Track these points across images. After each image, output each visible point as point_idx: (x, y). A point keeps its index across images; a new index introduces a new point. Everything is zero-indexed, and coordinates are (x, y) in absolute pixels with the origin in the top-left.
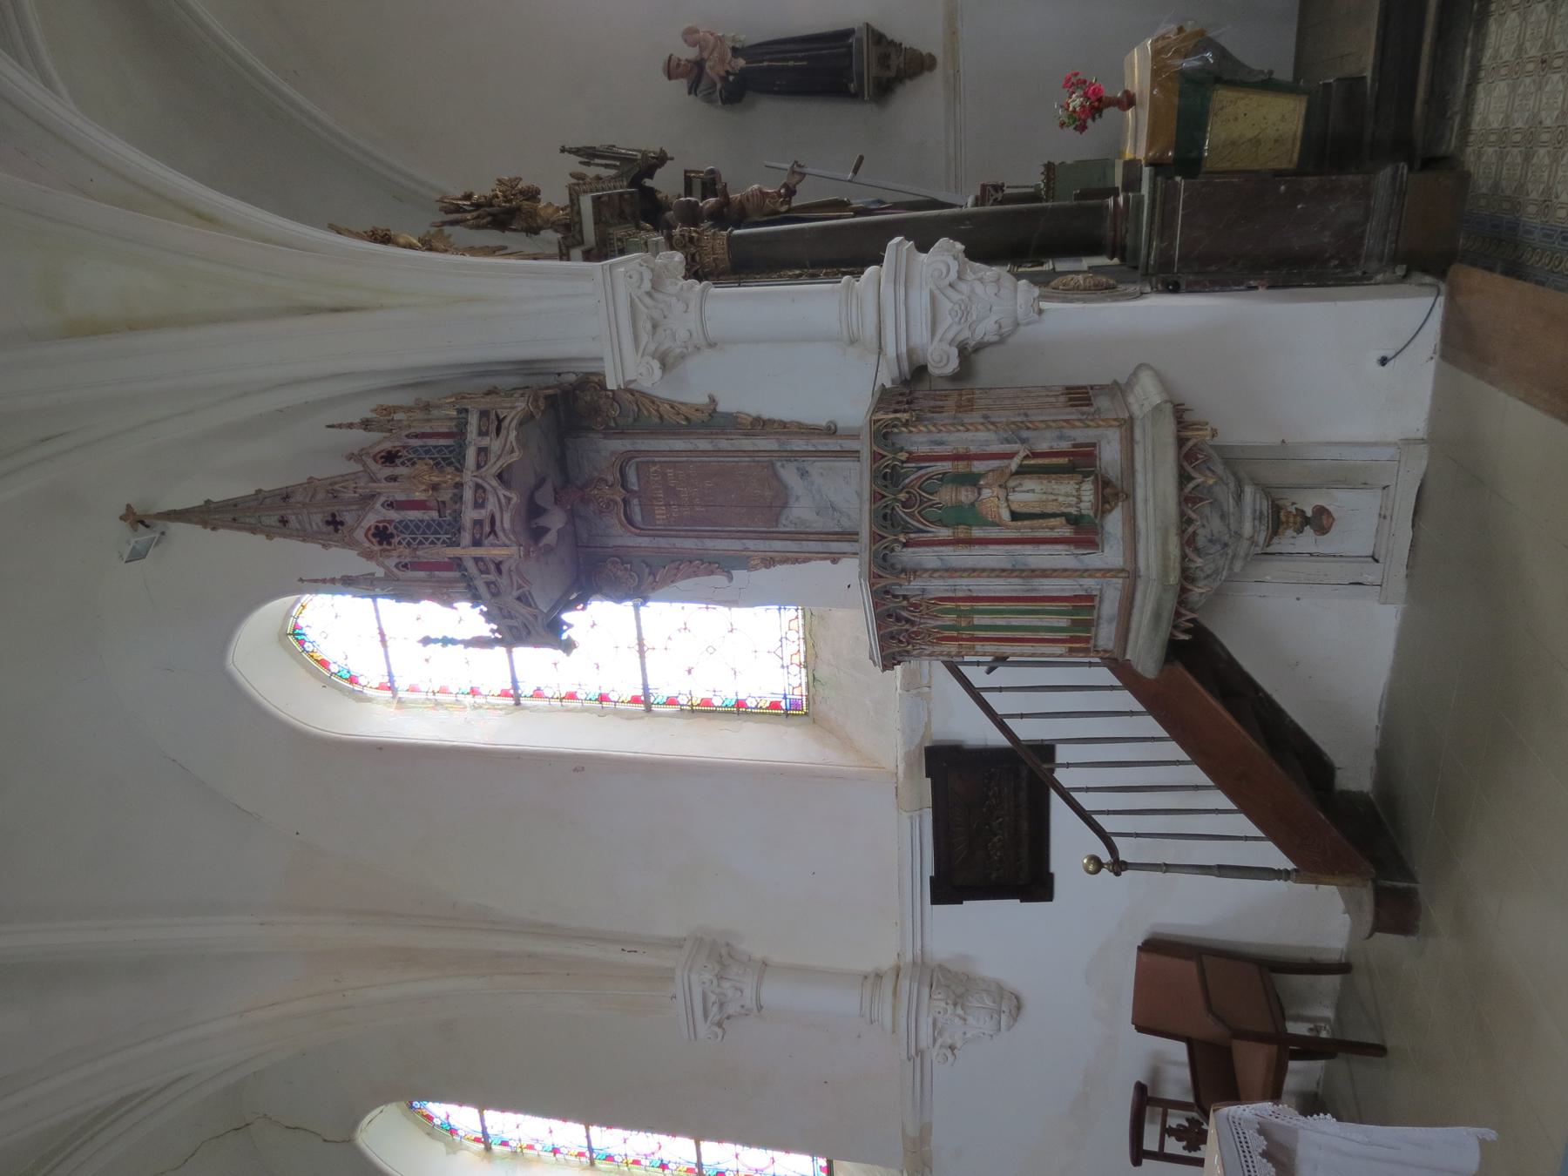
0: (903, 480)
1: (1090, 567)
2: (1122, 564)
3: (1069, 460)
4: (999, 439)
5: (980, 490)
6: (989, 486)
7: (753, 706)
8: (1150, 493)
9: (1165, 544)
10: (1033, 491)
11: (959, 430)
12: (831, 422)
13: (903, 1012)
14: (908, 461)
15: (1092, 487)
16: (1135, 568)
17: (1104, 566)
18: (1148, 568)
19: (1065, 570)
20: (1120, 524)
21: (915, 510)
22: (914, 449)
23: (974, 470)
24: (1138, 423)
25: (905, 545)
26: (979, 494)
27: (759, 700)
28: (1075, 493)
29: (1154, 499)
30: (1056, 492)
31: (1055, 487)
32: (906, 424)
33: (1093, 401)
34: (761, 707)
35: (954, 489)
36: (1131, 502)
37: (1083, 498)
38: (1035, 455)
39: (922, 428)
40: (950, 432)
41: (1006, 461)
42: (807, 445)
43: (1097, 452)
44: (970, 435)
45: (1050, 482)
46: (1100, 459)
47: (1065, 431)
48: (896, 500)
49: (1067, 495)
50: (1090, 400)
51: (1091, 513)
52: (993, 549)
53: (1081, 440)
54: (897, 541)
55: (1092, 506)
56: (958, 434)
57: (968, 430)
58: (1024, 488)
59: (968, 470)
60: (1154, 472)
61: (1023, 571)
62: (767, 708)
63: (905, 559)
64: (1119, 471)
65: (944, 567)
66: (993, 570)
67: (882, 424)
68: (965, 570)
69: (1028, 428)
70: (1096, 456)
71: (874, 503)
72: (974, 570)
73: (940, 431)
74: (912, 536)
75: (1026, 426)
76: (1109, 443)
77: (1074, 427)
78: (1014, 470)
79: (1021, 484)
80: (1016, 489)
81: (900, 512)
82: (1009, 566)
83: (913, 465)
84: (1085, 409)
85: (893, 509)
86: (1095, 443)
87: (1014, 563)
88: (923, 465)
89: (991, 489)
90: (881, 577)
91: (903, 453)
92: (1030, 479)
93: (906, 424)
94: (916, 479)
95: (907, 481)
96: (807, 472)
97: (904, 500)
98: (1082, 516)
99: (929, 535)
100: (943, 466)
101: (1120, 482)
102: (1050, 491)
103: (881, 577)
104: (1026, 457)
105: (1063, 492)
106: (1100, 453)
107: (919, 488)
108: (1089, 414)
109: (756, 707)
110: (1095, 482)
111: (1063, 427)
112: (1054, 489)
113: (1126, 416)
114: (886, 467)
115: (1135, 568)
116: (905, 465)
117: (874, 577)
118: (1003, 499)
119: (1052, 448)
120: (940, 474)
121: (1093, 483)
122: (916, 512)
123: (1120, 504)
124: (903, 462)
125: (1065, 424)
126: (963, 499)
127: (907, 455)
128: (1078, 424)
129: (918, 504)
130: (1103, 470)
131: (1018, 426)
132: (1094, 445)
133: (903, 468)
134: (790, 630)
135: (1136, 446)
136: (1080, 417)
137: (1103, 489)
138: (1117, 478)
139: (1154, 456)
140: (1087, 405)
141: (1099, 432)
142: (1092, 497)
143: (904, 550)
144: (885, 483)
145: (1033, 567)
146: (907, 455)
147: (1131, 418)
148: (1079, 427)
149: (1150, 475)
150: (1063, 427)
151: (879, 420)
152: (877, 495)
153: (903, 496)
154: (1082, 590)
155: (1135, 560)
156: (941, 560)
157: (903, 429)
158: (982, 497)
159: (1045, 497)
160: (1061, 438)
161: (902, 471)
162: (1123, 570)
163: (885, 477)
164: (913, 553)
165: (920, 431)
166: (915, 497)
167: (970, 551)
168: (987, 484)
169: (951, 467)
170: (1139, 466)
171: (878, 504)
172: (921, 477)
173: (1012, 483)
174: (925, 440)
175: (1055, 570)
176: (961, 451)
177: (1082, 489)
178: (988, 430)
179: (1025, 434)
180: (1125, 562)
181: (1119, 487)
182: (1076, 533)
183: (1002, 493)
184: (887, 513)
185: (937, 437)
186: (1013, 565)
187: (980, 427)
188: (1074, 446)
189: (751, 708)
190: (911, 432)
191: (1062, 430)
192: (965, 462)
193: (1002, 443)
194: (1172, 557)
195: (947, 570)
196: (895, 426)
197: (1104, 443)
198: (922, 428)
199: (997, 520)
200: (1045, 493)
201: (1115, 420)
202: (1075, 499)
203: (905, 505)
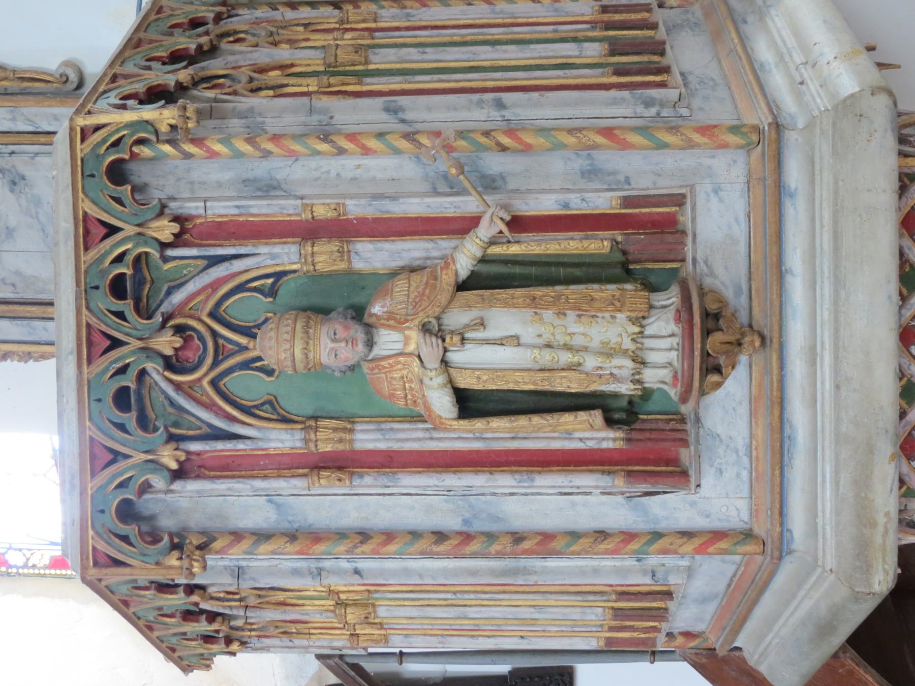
0: (169, 293)
1: (662, 526)
2: (745, 516)
3: (614, 241)
4: (426, 178)
5: (369, 329)
6: (396, 322)
7: (21, 564)
8: (825, 337)
9: (862, 482)
10: (515, 340)
11: (319, 153)
12: (67, 64)
13: (405, 622)
14: (179, 240)
15: (673, 327)
16: (781, 534)
17: (699, 522)
18: (813, 531)
19: (602, 535)
20: (744, 409)
21: (202, 376)
22: (192, 208)
23: (359, 265)
24: (792, 138)
25: (179, 474)
26: (370, 344)
27: (28, 554)
28: (628, 344)
29: (836, 358)
30: (578, 341)
31: (571, 330)
32: (174, 135)
33: (669, 59)
34: (34, 566)
35: (299, 326)
36: (775, 357)
37: (652, 357)
38: (518, 224)
39: (218, 147)
40: (293, 155)
41: (445, 244)
42: (14, 119)
43: (685, 219)
44: (348, 165)
45: (561, 314)
46: (694, 236)
47: (598, 155)
48: (148, 352)
49: (609, 352)
50: (659, 49)
51: (673, 393)
52: (410, 481)
53: (644, 185)
54: (156, 465)
55: (675, 377)
56: (313, 163)
57: (341, 151)
58: (490, 333)
59: (342, 266)
60: (838, 282)
61: (491, 537)
62: (45, 567)
63: (184, 503)
64: (743, 271)
65: (285, 525)
66: (415, 535)
67: (104, 140)
68: (341, 535)
69: (504, 149)
70: (684, 233)
71: (89, 362)
72: (364, 536)
73: (267, 154)
74: (195, 447)
75: (499, 144)
76: (716, 192)
77: (625, 146)
78: (464, 274)
79: (482, 324)
80: (467, 335)
81: (164, 385)
82: (452, 522)
83: (194, 252)
84: (654, 93)
85: (143, 373)
86: (683, 196)
87: (467, 515)
88: (220, 251)
89: (401, 330)
90: (117, 563)
91: (164, 222)
92: (507, 305)
93: (174, 135)
94: (204, 289)
95: (178, 297)
96: (23, 178)
97: (169, 352)
98: (647, 394)
99: (241, 445)
100: (273, 256)
101: (744, 299)
102: (561, 339)
103: (117, 563)
104: (492, 242)
105: (595, 344)
106: (694, 219)
107: (212, 315)
108: (662, 105)
109: (25, 566)
110: (684, 313)
111: (595, 147)
112: (571, 335)
113: (764, 120)
114: (119, 259)
115: (781, 534)
116: (170, 252)
117: (96, 564)
118: (432, 362)
119: (566, 206)
120: (267, 276)
121: (678, 319)
122: (205, 383)
123: (743, 359)
124: (164, 246)
125: (600, 140)
126: (325, 360)
127: (175, 228)
128: (635, 139)
129: (209, 361)
130: (701, 267)
131: (474, 142)
132: (678, 200)
133: (165, 259)
134: (44, 475)
135: (788, 204)
136: (640, 110)
137: (707, 332)
138: (738, 291)
139: (836, 237)
140: (662, 85)
141: (687, 160)
142: (673, 355)
143: (177, 485)
144: (118, 305)
145: (518, 524)
146: (175, 228)
147: (777, 127)
148: (642, 148)
149: (826, 290)
150: (595, 147)
151: (97, 128)
152: (97, 338)
153: (166, 343)
154: (645, 572)
155: (781, 514)
156: (278, 506)
157: (167, 148)
158: (377, 351)
159: (546, 358)
160: (591, 173)
161: (167, 266)
162: (748, 535)
163: (118, 288)
164: (200, 494)
165: (213, 155)
166: (201, 338)
167: (352, 486)
168: (391, 316)
169: (295, 258)
170: (795, 259)
171: (102, 363)
172: (215, 285)
173: (457, 318)
174: (227, 176)
175: (575, 535)
176: (322, 212)
177: (649, 331)
178: (397, 152)
179: (494, 163)
180: (754, 512)
181: (743, 318)
182: (629, 440)
183: (431, 350)
184: (127, 389)
185: (260, 169)
186: (466, 522)
187: (373, 143)
188: (627, 202)
189: (17, 567)
190: (188, 156)
191: (594, 153)
192: (334, 246)
193: (436, 193)
194: (881, 520)
195: (292, 536)
196: (141, 142)
197: (703, 189)
198: (218, 147)
199: (420, 409)
200: (549, 346)
201: (735, 129)
202: (629, 364)
203: (171, 364)
